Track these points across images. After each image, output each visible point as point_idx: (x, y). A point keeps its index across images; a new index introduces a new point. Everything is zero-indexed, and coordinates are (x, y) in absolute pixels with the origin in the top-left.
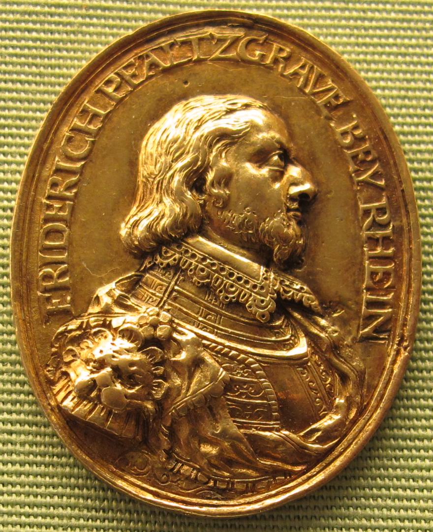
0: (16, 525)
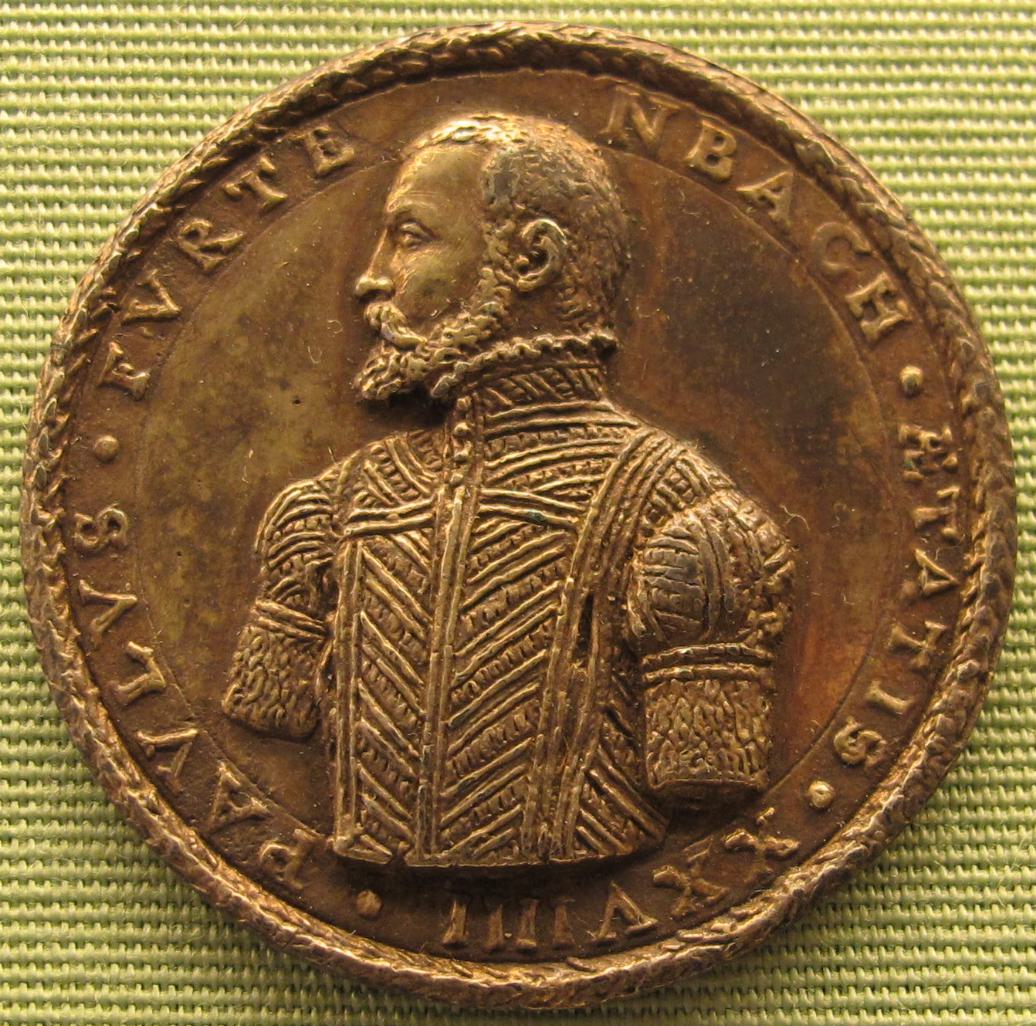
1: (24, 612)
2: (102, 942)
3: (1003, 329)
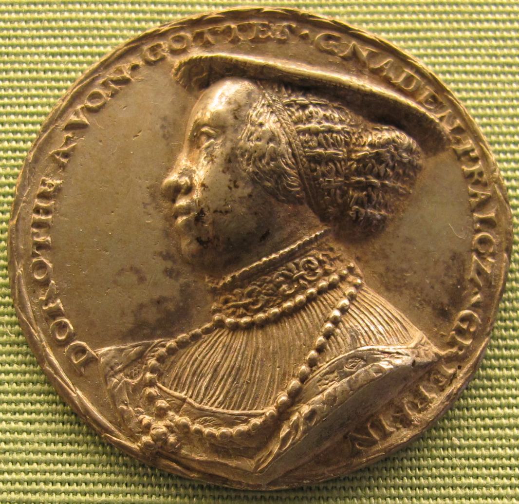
0: (19, 492)
1: (11, 300)
2: (50, 463)
3: (505, 165)
